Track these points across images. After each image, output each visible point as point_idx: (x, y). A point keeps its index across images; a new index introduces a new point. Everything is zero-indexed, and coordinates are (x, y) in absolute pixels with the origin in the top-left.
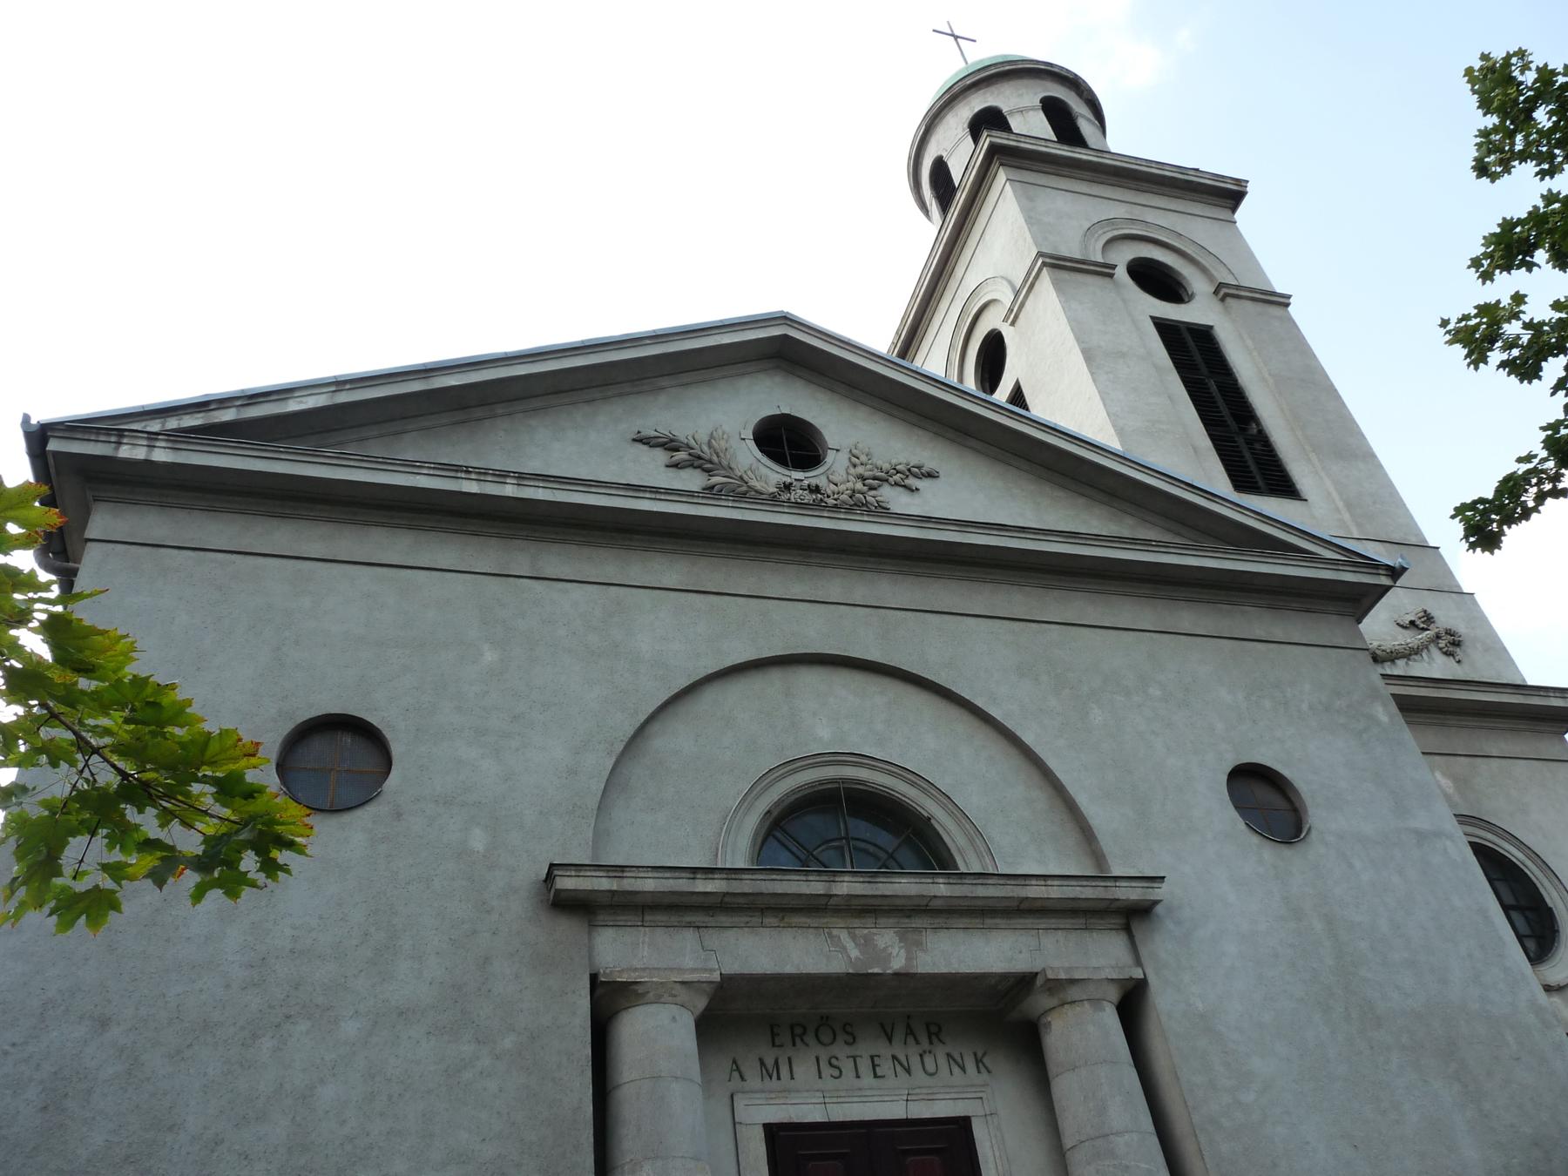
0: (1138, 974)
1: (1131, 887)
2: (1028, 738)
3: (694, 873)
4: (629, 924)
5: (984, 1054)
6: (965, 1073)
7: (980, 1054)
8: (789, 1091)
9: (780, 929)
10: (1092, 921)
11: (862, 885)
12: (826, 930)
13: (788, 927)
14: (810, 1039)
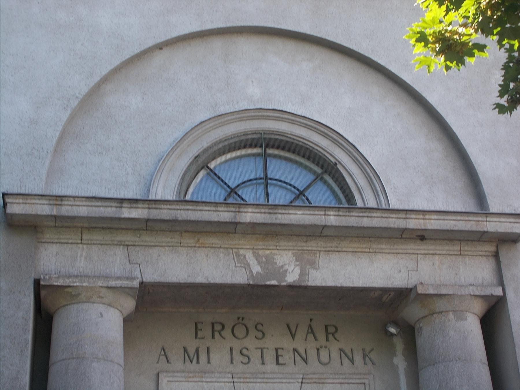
0: (498, 292)
1: (500, 222)
2: (432, 99)
3: (239, 208)
4: (70, 241)
5: (371, 351)
6: (353, 364)
7: (368, 349)
8: (205, 373)
9: (196, 248)
10: (466, 248)
11: (263, 215)
12: (234, 250)
13: (203, 247)
14: (227, 333)
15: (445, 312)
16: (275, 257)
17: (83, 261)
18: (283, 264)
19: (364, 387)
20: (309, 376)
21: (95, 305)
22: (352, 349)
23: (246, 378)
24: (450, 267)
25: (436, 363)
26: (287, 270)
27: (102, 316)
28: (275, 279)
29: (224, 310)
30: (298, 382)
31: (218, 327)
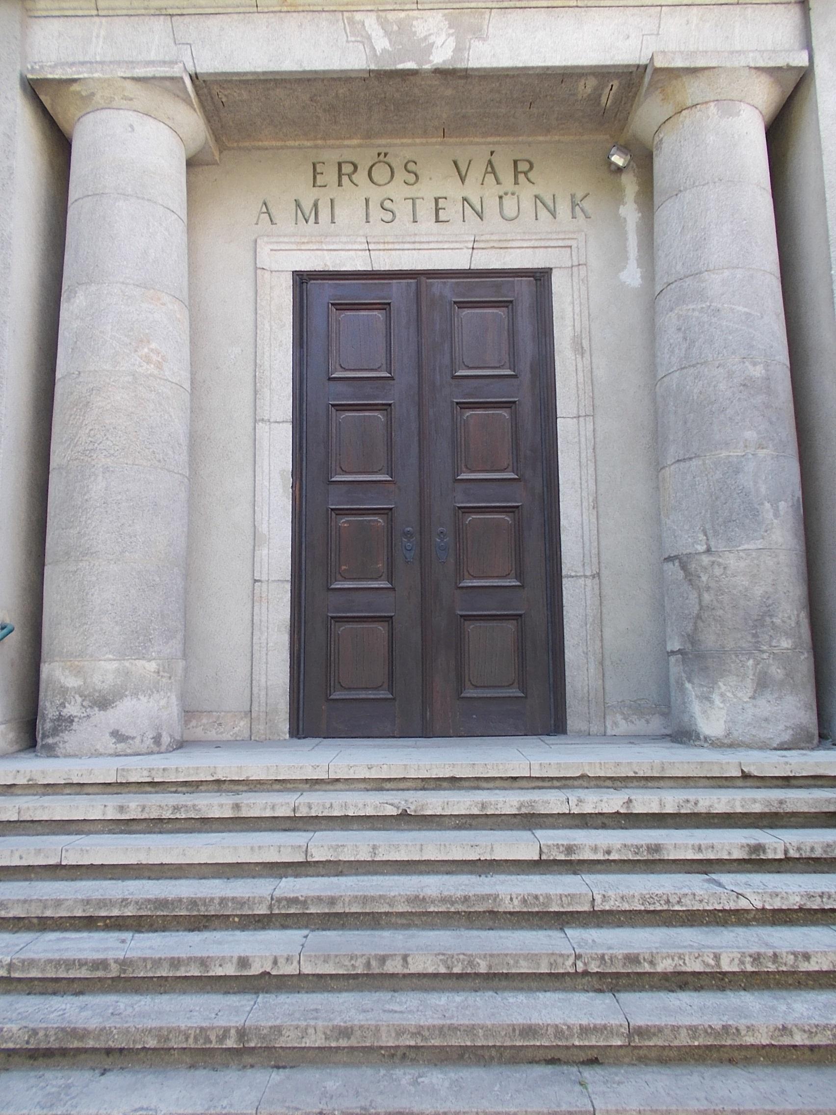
0: (801, 59)
4: (80, 13)
6: (555, 218)
9: (282, 15)
12: (346, 14)
14: (361, 177)
15: (703, 104)
16: (415, 23)
17: (101, 43)
18: (428, 33)
19: (569, 252)
20: (483, 238)
21: (121, 112)
22: (554, 196)
23: (388, 243)
24: (717, 26)
25: (680, 191)
26: (434, 43)
27: (133, 130)
28: (413, 60)
29: (355, 142)
30: (468, 248)
31: (347, 169)
